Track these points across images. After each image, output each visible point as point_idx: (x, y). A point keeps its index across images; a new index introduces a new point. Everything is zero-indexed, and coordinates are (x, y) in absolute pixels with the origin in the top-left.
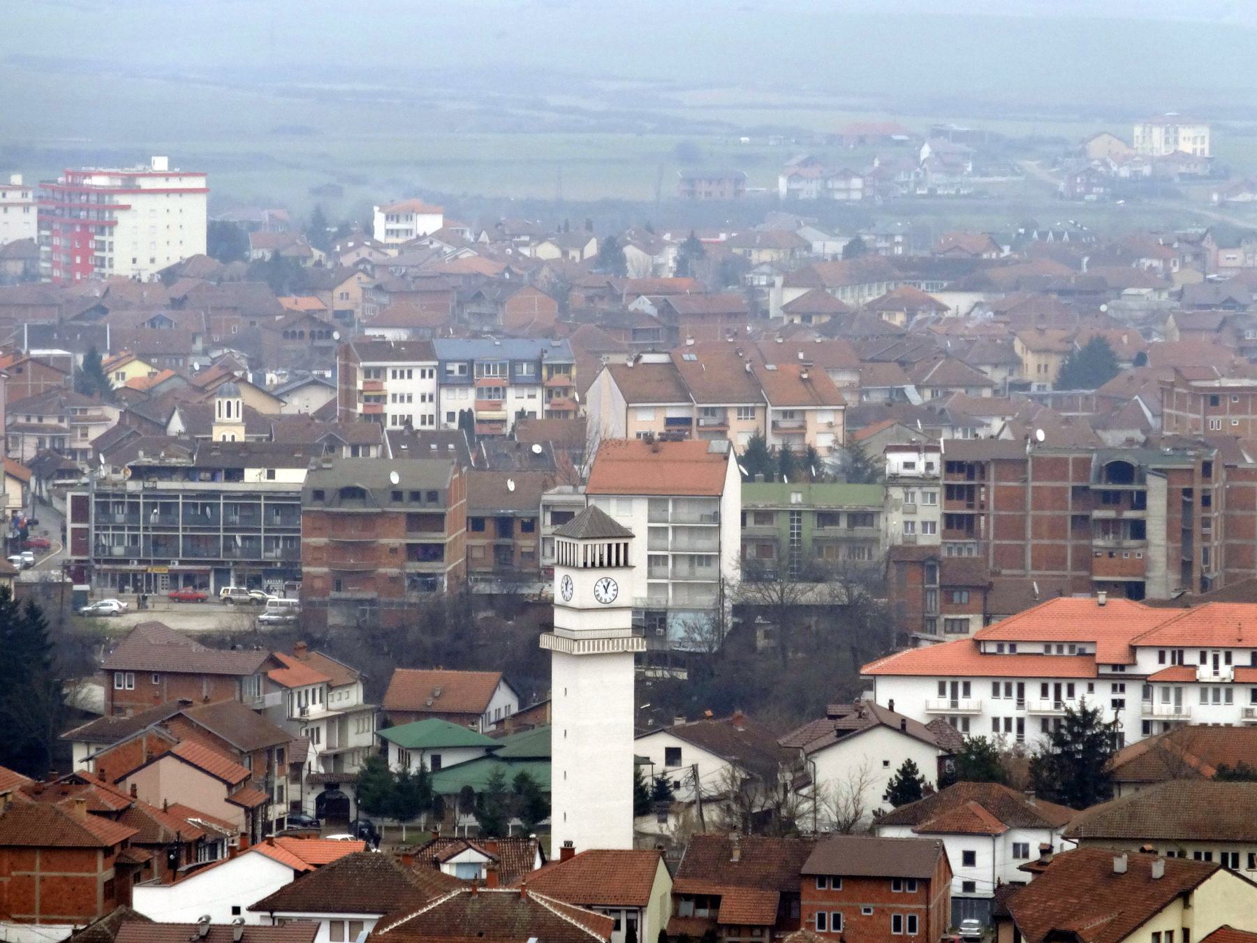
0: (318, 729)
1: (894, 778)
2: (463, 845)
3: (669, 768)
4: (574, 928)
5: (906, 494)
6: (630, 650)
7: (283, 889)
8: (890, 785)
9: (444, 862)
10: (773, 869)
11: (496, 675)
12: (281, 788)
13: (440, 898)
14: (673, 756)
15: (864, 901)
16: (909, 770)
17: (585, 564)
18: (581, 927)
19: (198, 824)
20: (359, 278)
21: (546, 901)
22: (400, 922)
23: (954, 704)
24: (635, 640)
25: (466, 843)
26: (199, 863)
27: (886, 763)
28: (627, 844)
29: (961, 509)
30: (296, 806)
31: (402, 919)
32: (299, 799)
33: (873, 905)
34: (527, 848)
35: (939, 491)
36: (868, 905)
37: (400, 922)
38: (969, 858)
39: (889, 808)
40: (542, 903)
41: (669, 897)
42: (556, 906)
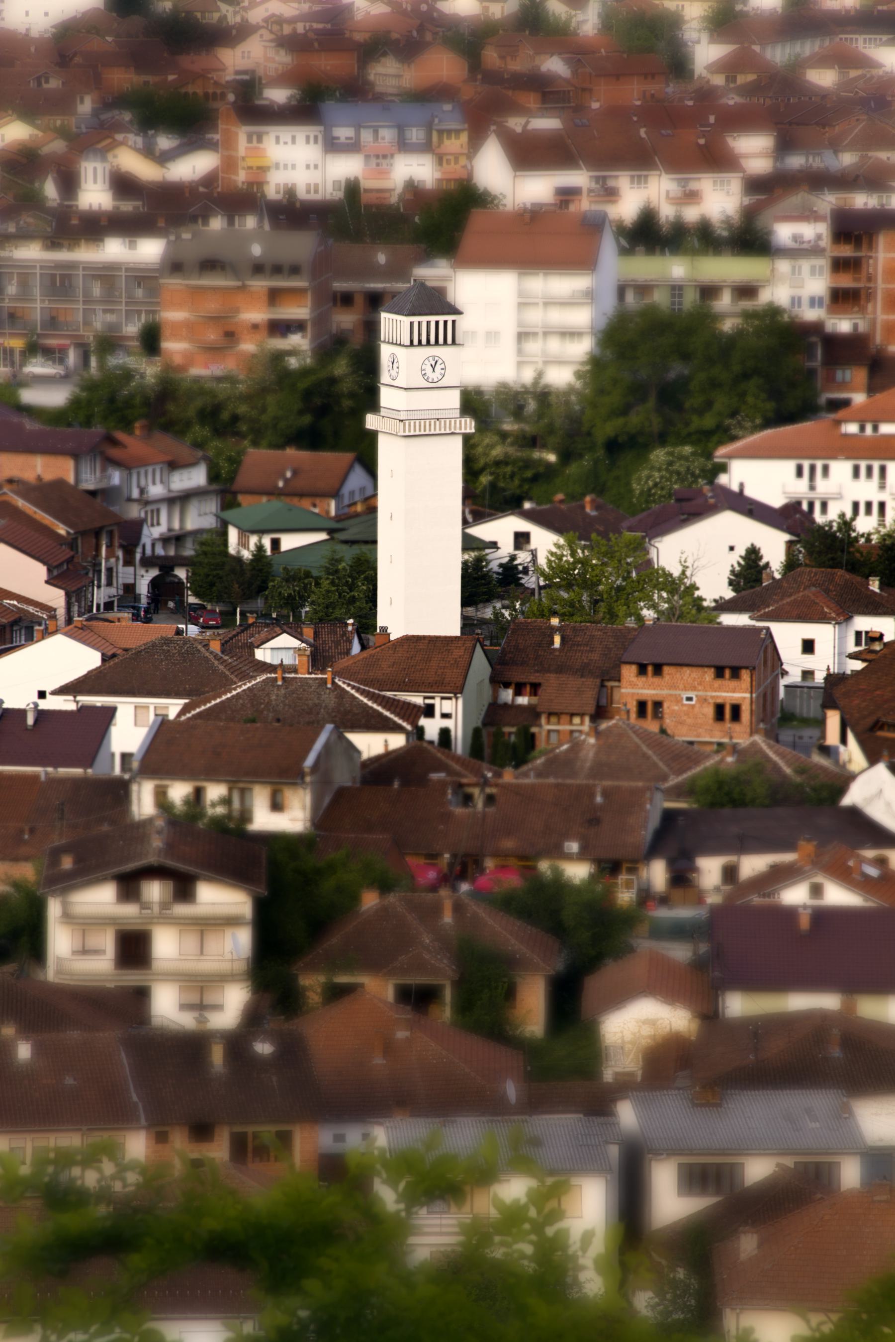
0: (158, 511)
1: (736, 565)
2: (278, 629)
3: (516, 552)
4: (380, 714)
5: (794, 268)
6: (458, 431)
7: (89, 672)
8: (733, 572)
9: (258, 647)
10: (595, 656)
11: (348, 456)
12: (110, 570)
13: (245, 684)
14: (522, 539)
15: (685, 689)
16: (753, 554)
17: (412, 341)
18: (387, 714)
19: (14, 606)
20: (261, 36)
21: (353, 687)
22: (203, 708)
23: (812, 488)
24: (463, 420)
25: (281, 628)
26: (14, 644)
27: (732, 549)
28: (455, 630)
29: (846, 281)
30: (130, 589)
31: (205, 705)
32: (132, 581)
33: (696, 693)
34: (344, 634)
35: (823, 263)
36: (690, 694)
37: (203, 708)
38: (808, 646)
39: (729, 594)
40: (348, 689)
41: (487, 681)
42: (362, 692)
